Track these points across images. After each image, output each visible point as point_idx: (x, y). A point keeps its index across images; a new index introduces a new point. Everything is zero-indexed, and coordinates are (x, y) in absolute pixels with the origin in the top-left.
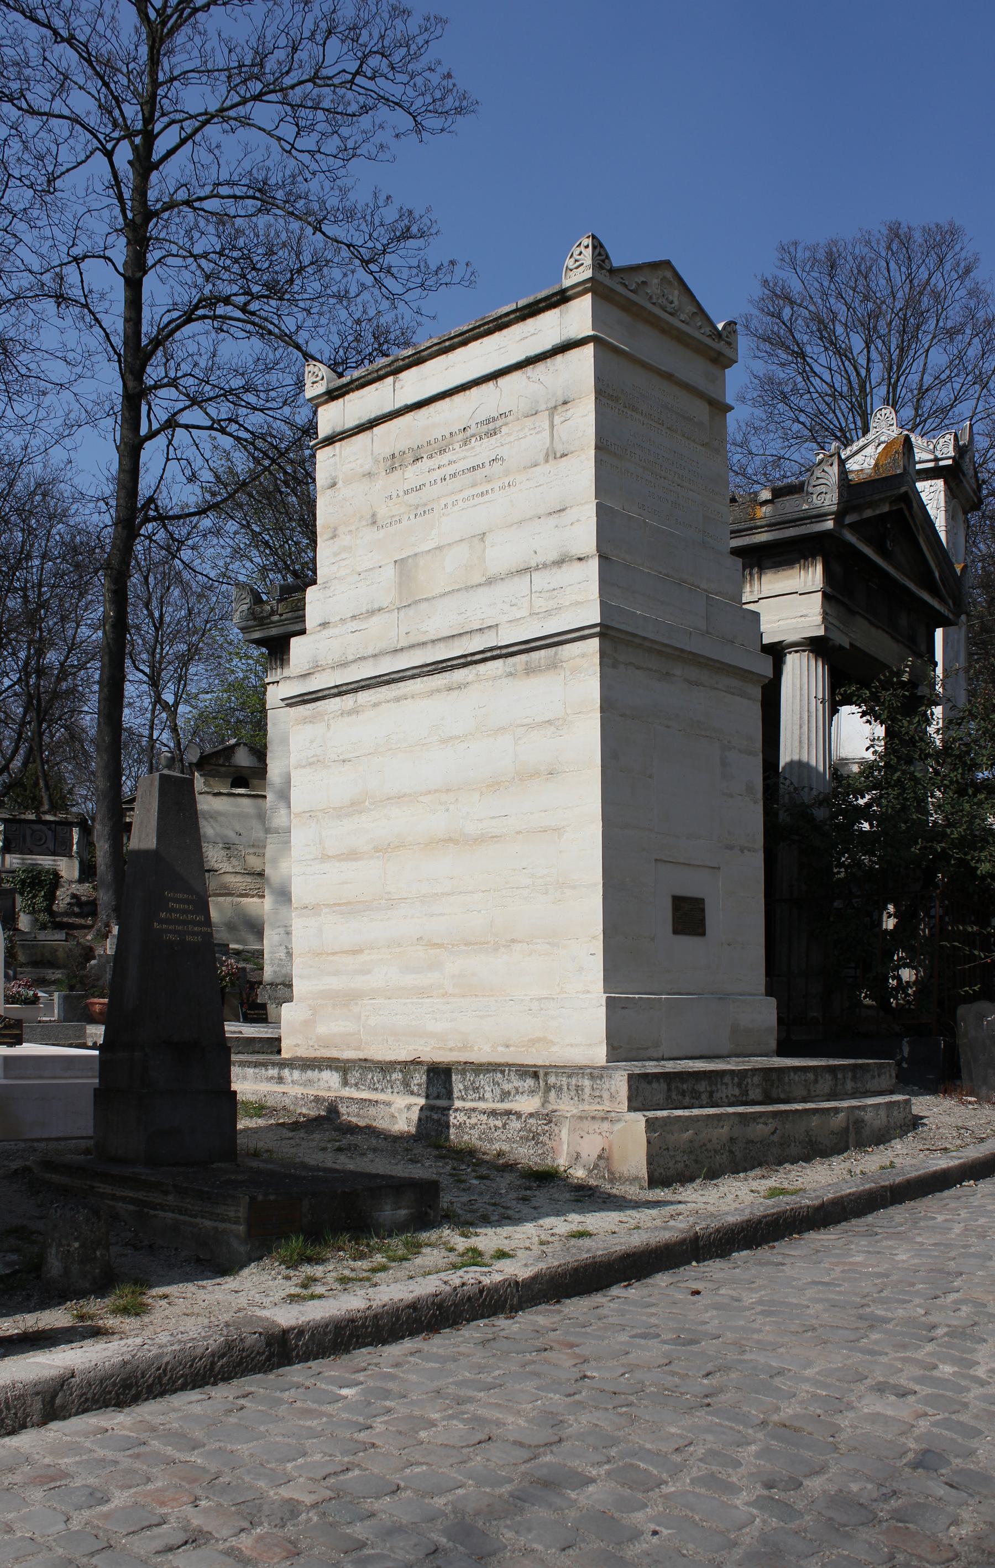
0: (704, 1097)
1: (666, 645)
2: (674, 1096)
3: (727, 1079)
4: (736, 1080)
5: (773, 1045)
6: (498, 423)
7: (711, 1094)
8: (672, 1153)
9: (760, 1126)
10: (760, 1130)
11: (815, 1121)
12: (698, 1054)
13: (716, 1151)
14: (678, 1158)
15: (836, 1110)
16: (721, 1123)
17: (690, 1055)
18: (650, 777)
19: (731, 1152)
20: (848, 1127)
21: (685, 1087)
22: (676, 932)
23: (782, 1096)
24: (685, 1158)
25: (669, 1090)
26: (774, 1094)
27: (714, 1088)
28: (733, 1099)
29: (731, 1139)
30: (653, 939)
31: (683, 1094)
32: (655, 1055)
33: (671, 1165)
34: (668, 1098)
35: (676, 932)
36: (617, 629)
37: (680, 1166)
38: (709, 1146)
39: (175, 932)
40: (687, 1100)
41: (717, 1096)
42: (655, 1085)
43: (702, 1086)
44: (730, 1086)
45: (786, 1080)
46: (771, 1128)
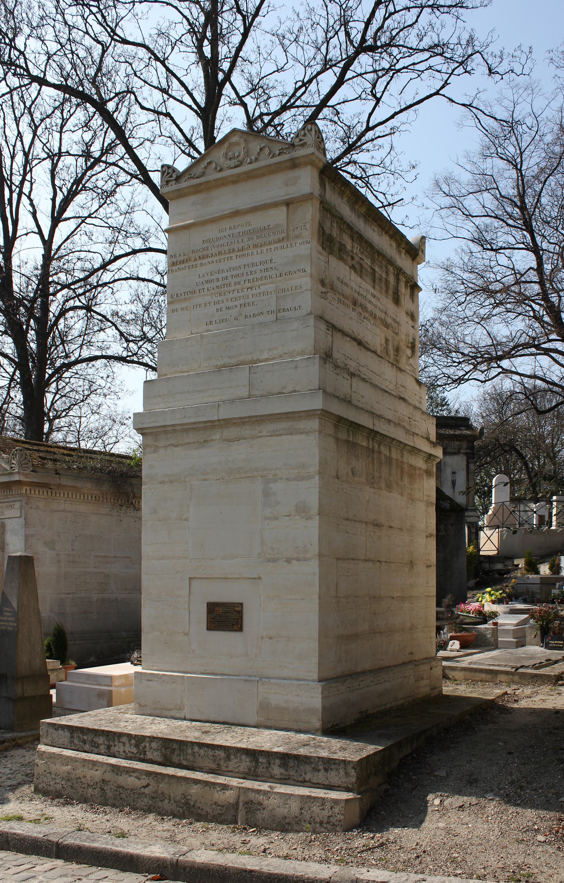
0: (103, 748)
1: (195, 423)
2: (76, 741)
3: (124, 739)
4: (133, 741)
5: (317, 724)
6: (256, 283)
7: (109, 747)
8: (54, 777)
9: (132, 778)
10: (131, 781)
11: (194, 790)
12: (222, 720)
13: (88, 785)
14: (58, 781)
15: (225, 787)
16: (96, 768)
17: (212, 719)
18: (186, 520)
19: (102, 789)
20: (237, 803)
21: (85, 737)
22: (209, 628)
23: (185, 763)
24: (63, 782)
25: (72, 737)
26: (175, 759)
27: (111, 743)
28: (129, 754)
29: (103, 780)
30: (186, 634)
31: (84, 742)
32: (178, 715)
33: (52, 783)
34: (71, 742)
35: (209, 628)
36: (148, 428)
37: (59, 787)
38: (83, 780)
39: (4, 625)
40: (87, 747)
41: (114, 749)
42: (60, 732)
43: (100, 740)
44: (127, 745)
45: (190, 751)
46: (144, 782)
